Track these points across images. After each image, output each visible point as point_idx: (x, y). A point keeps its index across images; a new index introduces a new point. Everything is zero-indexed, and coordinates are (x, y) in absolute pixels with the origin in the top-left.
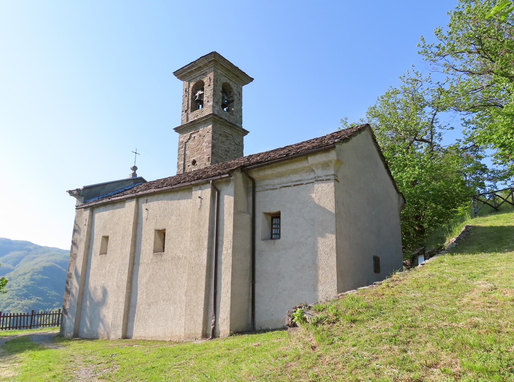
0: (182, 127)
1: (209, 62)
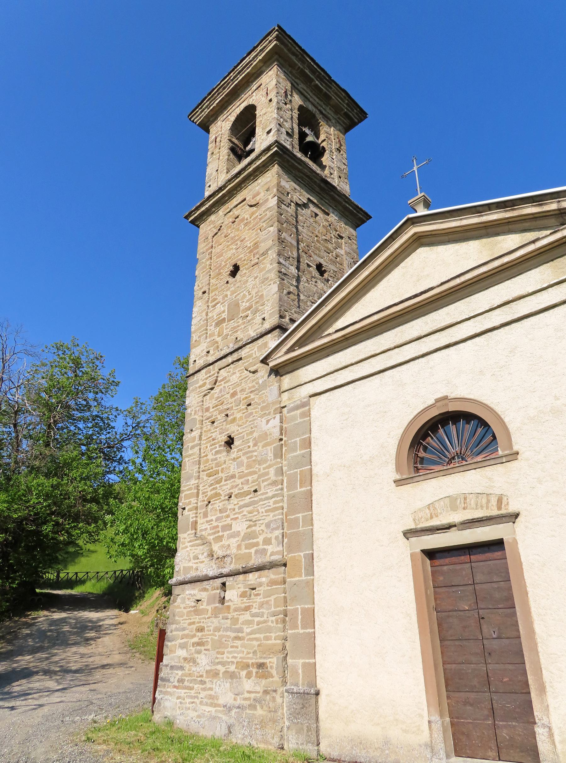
0: (299, 164)
1: (346, 114)
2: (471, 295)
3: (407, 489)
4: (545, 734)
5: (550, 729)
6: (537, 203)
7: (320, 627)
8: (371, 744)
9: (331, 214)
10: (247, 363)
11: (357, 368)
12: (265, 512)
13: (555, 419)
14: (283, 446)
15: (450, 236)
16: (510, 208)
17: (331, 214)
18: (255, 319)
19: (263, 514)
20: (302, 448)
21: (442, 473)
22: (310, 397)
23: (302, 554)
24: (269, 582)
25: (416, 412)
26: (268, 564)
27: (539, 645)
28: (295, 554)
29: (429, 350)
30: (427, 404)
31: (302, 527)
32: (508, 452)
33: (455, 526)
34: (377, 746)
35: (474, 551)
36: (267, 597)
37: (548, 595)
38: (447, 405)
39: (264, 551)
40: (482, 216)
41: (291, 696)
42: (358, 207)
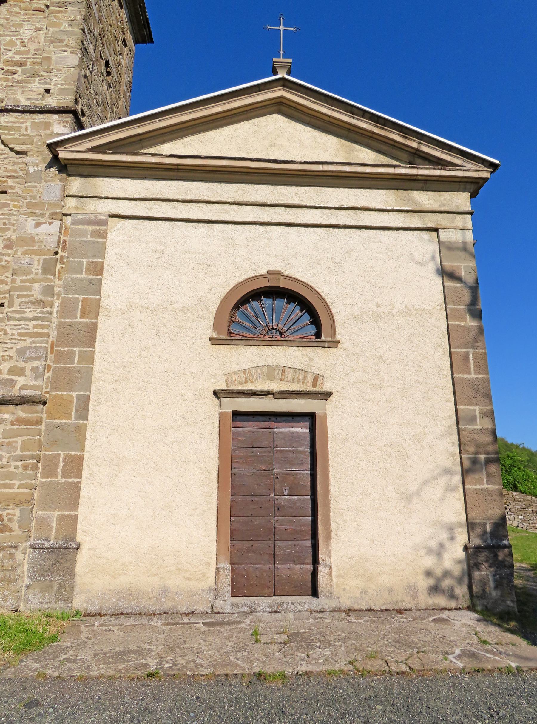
2: (322, 187)
3: (224, 350)
4: (326, 572)
5: (331, 567)
6: (403, 135)
7: (89, 477)
8: (143, 594)
9: (123, 10)
10: (9, 137)
11: (183, 207)
12: (18, 335)
13: (375, 322)
14: (58, 261)
15: (312, 120)
16: (380, 126)
17: (123, 10)
18: (31, 83)
19: (13, 337)
20: (88, 272)
21: (264, 343)
22: (110, 216)
23: (74, 394)
24: (16, 420)
25: (245, 277)
26: (19, 398)
27: (331, 502)
28: (63, 393)
29: (271, 221)
30: (258, 272)
31: (79, 363)
32: (330, 339)
33: (273, 394)
34: (151, 596)
35: (279, 419)
36: (10, 438)
37: (345, 463)
38: (279, 280)
39: (11, 383)
40: (354, 118)
41: (37, 552)
42: (147, 21)
